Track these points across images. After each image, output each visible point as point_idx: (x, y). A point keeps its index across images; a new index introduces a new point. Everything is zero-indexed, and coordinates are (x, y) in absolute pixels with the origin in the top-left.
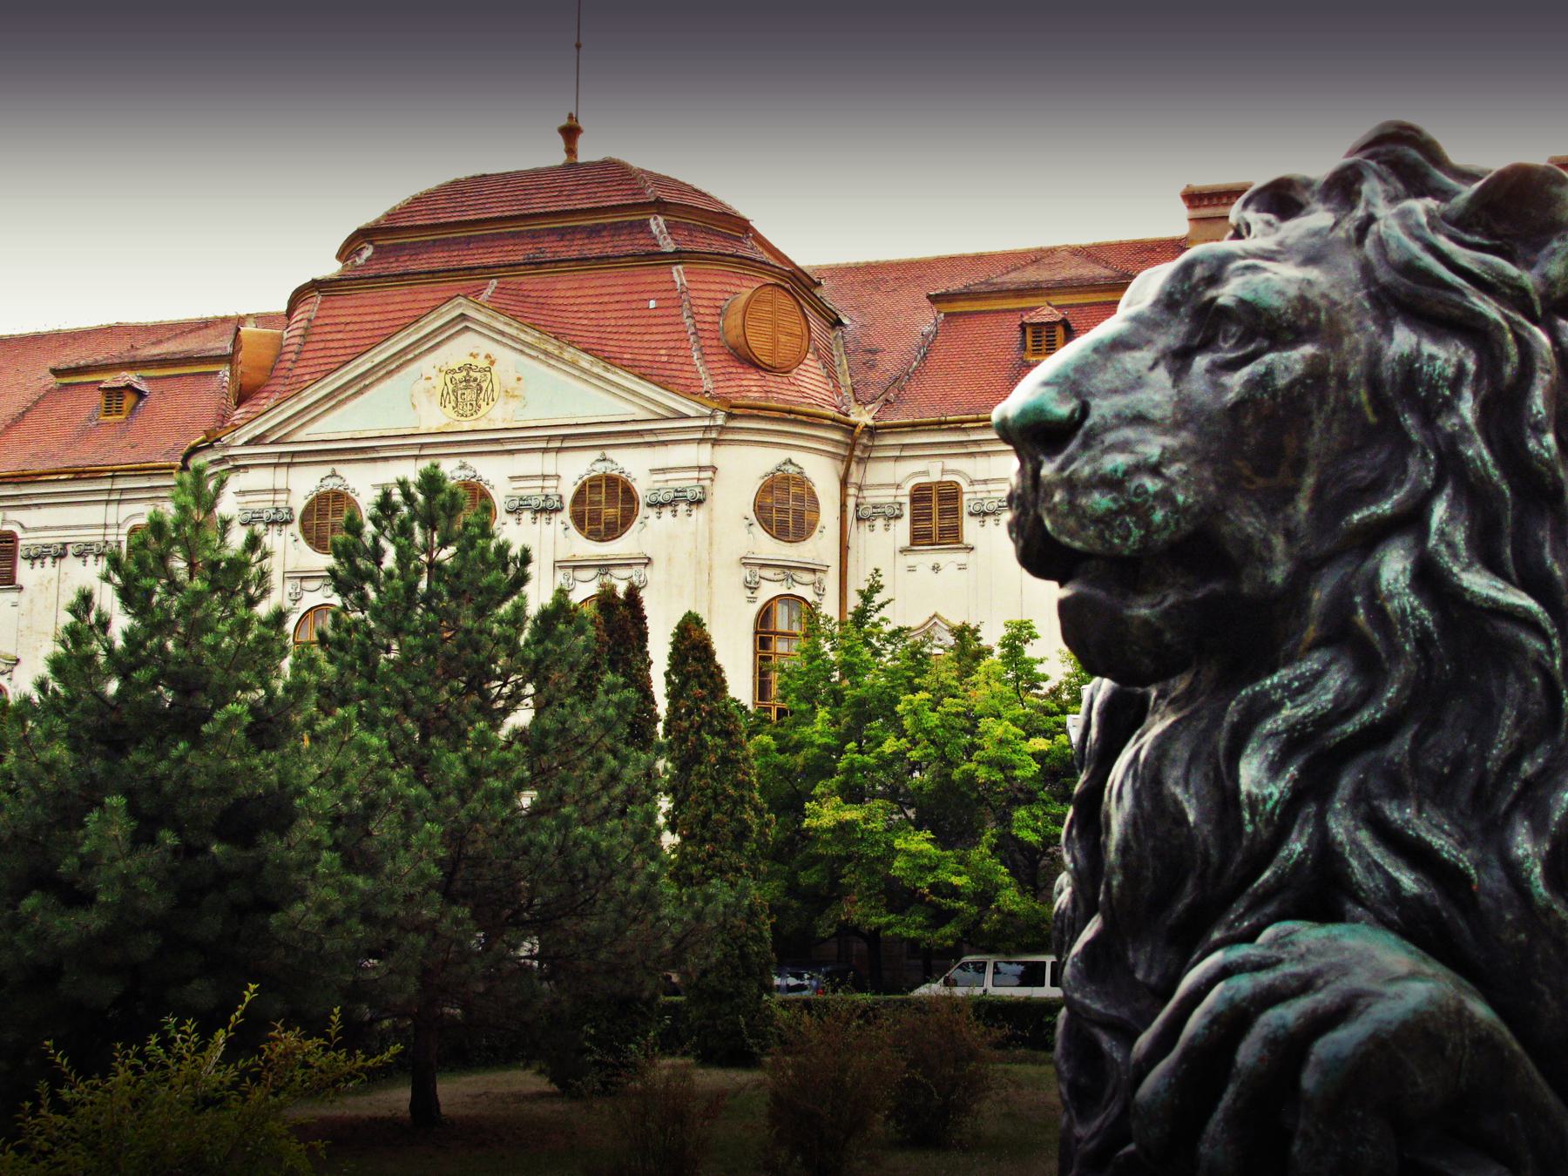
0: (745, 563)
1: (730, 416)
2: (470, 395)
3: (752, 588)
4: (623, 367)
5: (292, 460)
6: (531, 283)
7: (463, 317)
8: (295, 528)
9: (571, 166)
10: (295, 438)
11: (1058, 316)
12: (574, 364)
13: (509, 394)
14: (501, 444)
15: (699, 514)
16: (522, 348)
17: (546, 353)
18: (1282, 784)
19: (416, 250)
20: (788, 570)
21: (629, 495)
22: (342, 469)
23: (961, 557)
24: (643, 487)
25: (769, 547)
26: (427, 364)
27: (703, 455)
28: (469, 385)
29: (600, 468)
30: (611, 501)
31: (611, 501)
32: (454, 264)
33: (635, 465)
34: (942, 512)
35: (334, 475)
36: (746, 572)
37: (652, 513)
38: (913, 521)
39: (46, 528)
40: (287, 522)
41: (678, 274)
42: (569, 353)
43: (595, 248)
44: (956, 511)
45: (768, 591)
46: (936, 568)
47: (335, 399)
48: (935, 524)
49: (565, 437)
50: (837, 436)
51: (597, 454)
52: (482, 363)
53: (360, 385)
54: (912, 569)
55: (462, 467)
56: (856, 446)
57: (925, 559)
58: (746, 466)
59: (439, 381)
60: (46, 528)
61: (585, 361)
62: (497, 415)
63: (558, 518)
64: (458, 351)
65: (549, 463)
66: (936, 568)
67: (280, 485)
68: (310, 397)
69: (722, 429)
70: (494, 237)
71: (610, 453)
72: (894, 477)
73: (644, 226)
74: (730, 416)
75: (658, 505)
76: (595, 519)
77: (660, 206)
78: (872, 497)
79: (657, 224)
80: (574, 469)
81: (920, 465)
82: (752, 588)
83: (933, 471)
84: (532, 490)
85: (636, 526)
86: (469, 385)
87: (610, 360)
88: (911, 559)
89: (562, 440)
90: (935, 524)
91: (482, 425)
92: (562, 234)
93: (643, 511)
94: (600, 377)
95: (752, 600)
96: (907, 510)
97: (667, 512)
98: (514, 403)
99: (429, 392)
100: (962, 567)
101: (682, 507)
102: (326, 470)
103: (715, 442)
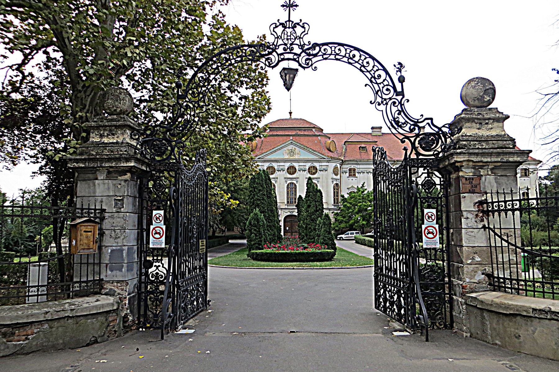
5: (265, 161)
9: (290, 119)
18: (282, 218)
24: (276, 168)
25: (335, 177)
26: (285, 149)
27: (327, 164)
28: (292, 152)
31: (314, 169)
33: (317, 165)
39: (514, 221)
45: (289, 182)
48: (352, 174)
56: (343, 163)
57: (351, 178)
58: (332, 165)
60: (514, 221)
62: (296, 157)
72: (346, 167)
75: (321, 170)
76: (312, 172)
77: (314, 127)
79: (314, 130)
80: (308, 165)
90: (352, 174)
92: (300, 130)
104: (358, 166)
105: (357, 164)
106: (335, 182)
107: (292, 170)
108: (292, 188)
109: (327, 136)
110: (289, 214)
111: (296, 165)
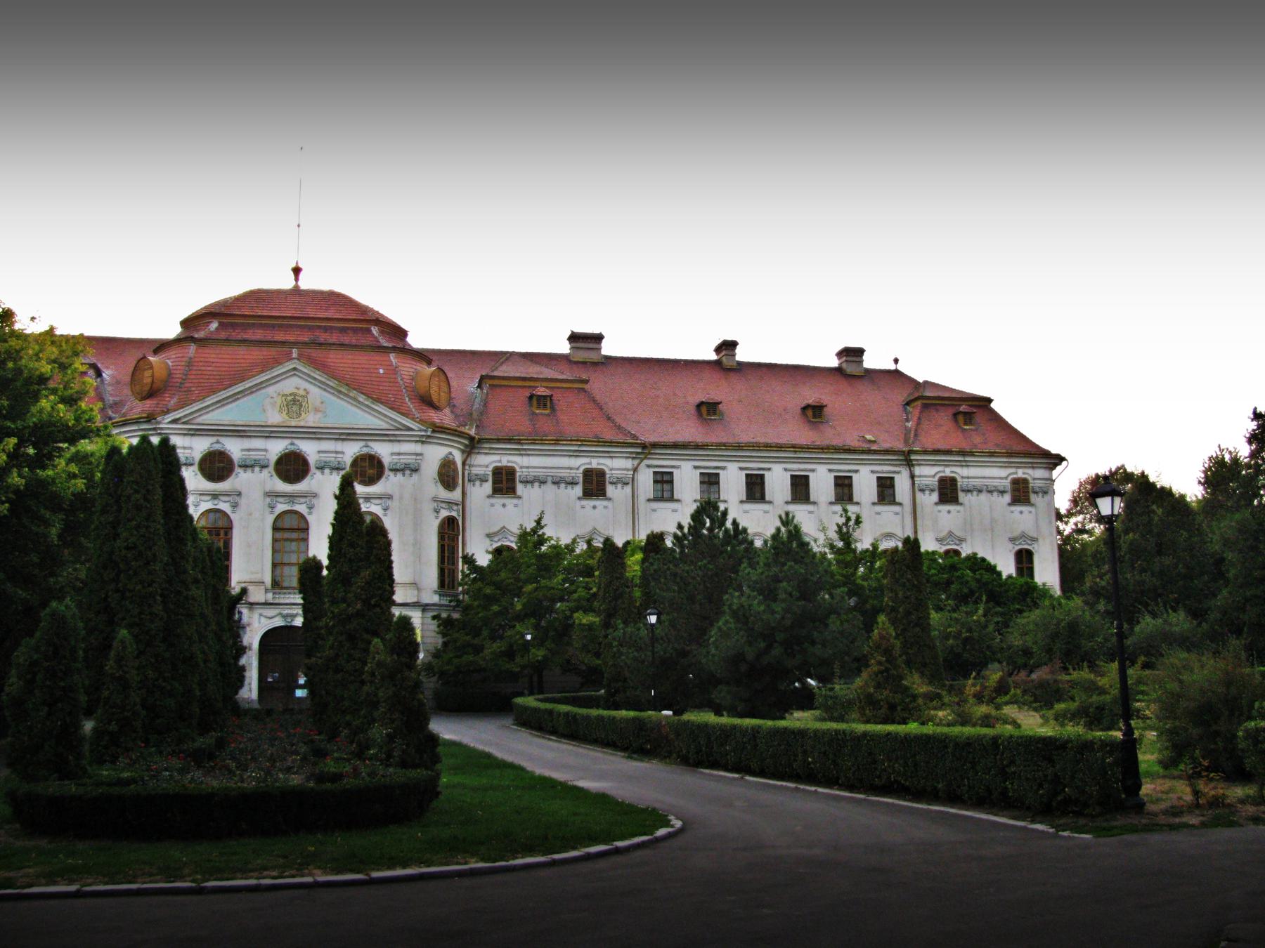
0: (268, 494)
1: (434, 431)
2: (295, 408)
3: (437, 511)
4: (382, 403)
6: (315, 353)
7: (295, 369)
8: (196, 468)
10: (199, 420)
11: (547, 392)
12: (355, 399)
13: (317, 410)
14: (314, 434)
15: (415, 476)
16: (324, 386)
17: (340, 392)
19: (245, 327)
20: (291, 497)
21: (305, 463)
22: (222, 440)
23: (515, 501)
25: (443, 494)
27: (417, 448)
29: (365, 450)
30: (372, 466)
32: (269, 338)
33: (384, 451)
34: (508, 480)
35: (218, 442)
36: (268, 500)
37: (392, 474)
38: (494, 483)
40: (192, 465)
41: (392, 356)
42: (353, 393)
43: (346, 339)
44: (514, 480)
45: (281, 507)
46: (504, 505)
47: (221, 403)
48: (504, 485)
49: (349, 434)
50: (466, 442)
51: (362, 443)
52: (302, 392)
53: (235, 397)
54: (583, 507)
55: (292, 444)
56: (473, 446)
58: (435, 454)
59: (279, 401)
61: (362, 398)
62: (310, 419)
63: (265, 471)
64: (291, 385)
65: (339, 446)
66: (594, 507)
67: (339, 449)
68: (209, 401)
69: (429, 437)
70: (281, 326)
71: (370, 444)
72: (486, 462)
73: (369, 331)
74: (434, 431)
75: (395, 470)
78: (475, 471)
80: (276, 448)
81: (496, 458)
82: (437, 511)
83: (505, 460)
84: (330, 458)
85: (383, 479)
86: (295, 403)
87: (378, 400)
88: (493, 501)
89: (269, 433)
90: (504, 485)
91: (302, 424)
92: (326, 329)
93: (387, 472)
94: (367, 406)
95: (272, 513)
96: (490, 479)
97: (249, 470)
98: (319, 415)
99: (274, 404)
100: (606, 507)
101: (408, 472)
102: (214, 439)
103: (423, 442)
104: (964, 472)
105: (521, 453)
106: (444, 513)
107: (292, 467)
108: (290, 529)
109: (424, 356)
110: (278, 622)
111: (310, 449)
